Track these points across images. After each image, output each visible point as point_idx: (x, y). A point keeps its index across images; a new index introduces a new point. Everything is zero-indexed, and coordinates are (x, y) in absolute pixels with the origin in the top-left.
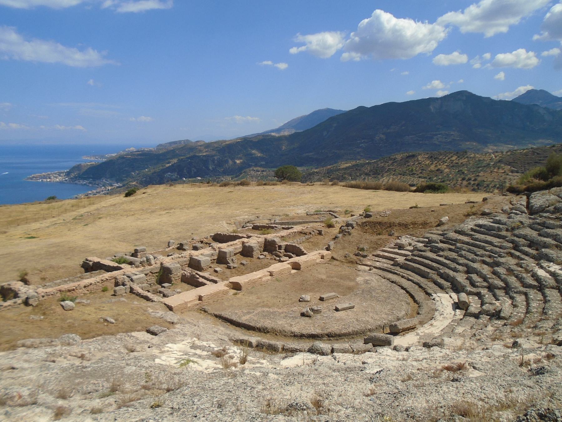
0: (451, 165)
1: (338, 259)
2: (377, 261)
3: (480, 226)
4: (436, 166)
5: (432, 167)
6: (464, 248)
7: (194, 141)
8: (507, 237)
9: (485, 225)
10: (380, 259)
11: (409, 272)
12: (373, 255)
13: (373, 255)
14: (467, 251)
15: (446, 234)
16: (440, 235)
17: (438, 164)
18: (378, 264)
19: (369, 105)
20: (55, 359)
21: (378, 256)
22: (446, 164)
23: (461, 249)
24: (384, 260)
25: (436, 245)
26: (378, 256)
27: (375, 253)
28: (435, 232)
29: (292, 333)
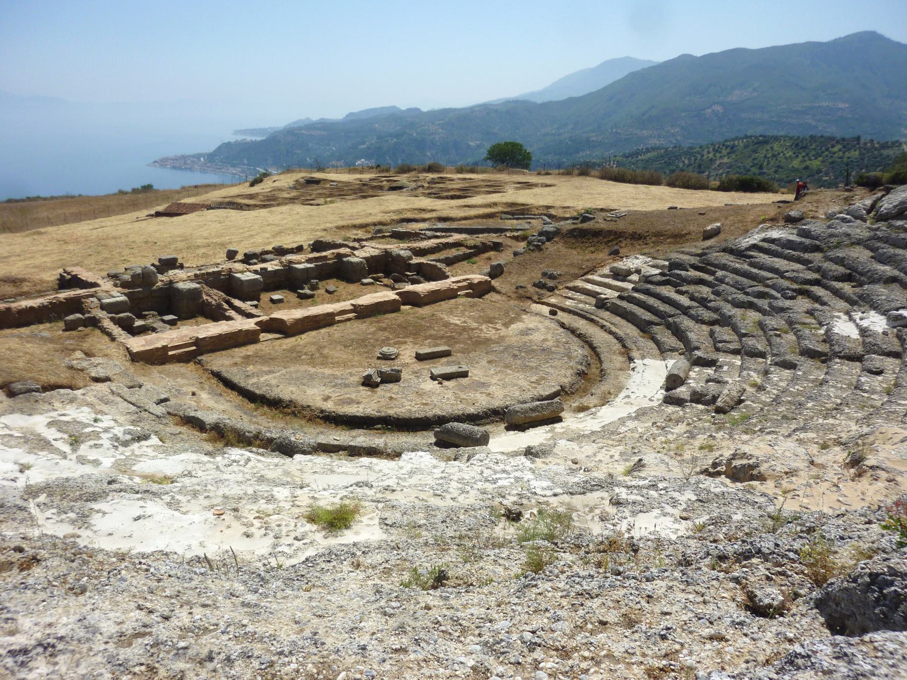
0: (830, 160)
1: (503, 291)
2: (570, 298)
3: (773, 241)
4: (803, 161)
5: (796, 163)
6: (727, 280)
7: (403, 108)
8: (811, 262)
9: (779, 239)
10: (578, 296)
11: (617, 320)
12: (567, 288)
13: (567, 288)
14: (732, 286)
15: (705, 254)
16: (698, 255)
17: (806, 158)
18: (568, 303)
19: (698, 52)
20: (755, 447)
21: (575, 289)
22: (820, 159)
23: (721, 281)
24: (583, 297)
25: (683, 273)
26: (575, 289)
27: (571, 285)
28: (687, 250)
29: (322, 411)
